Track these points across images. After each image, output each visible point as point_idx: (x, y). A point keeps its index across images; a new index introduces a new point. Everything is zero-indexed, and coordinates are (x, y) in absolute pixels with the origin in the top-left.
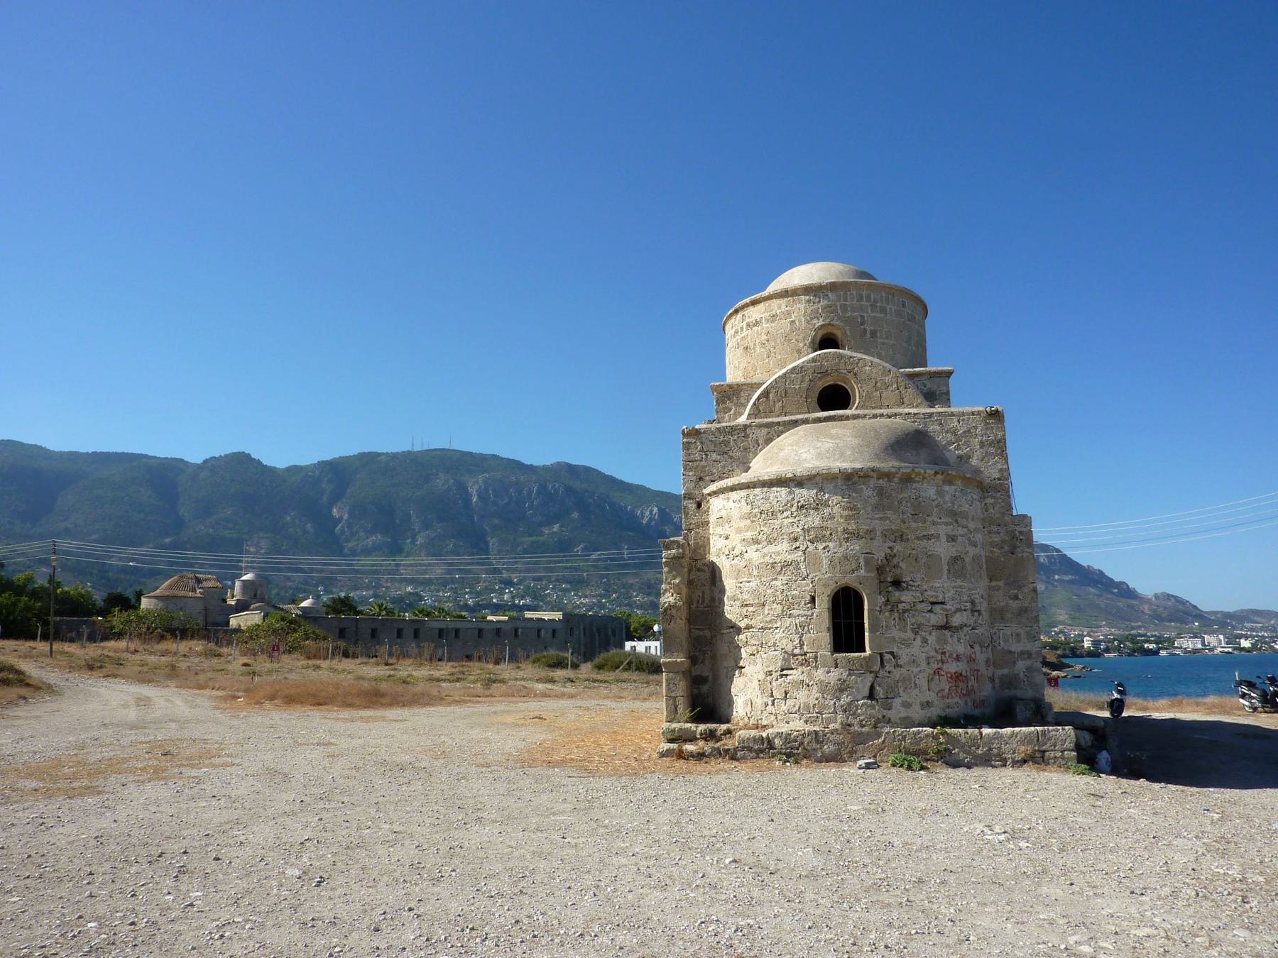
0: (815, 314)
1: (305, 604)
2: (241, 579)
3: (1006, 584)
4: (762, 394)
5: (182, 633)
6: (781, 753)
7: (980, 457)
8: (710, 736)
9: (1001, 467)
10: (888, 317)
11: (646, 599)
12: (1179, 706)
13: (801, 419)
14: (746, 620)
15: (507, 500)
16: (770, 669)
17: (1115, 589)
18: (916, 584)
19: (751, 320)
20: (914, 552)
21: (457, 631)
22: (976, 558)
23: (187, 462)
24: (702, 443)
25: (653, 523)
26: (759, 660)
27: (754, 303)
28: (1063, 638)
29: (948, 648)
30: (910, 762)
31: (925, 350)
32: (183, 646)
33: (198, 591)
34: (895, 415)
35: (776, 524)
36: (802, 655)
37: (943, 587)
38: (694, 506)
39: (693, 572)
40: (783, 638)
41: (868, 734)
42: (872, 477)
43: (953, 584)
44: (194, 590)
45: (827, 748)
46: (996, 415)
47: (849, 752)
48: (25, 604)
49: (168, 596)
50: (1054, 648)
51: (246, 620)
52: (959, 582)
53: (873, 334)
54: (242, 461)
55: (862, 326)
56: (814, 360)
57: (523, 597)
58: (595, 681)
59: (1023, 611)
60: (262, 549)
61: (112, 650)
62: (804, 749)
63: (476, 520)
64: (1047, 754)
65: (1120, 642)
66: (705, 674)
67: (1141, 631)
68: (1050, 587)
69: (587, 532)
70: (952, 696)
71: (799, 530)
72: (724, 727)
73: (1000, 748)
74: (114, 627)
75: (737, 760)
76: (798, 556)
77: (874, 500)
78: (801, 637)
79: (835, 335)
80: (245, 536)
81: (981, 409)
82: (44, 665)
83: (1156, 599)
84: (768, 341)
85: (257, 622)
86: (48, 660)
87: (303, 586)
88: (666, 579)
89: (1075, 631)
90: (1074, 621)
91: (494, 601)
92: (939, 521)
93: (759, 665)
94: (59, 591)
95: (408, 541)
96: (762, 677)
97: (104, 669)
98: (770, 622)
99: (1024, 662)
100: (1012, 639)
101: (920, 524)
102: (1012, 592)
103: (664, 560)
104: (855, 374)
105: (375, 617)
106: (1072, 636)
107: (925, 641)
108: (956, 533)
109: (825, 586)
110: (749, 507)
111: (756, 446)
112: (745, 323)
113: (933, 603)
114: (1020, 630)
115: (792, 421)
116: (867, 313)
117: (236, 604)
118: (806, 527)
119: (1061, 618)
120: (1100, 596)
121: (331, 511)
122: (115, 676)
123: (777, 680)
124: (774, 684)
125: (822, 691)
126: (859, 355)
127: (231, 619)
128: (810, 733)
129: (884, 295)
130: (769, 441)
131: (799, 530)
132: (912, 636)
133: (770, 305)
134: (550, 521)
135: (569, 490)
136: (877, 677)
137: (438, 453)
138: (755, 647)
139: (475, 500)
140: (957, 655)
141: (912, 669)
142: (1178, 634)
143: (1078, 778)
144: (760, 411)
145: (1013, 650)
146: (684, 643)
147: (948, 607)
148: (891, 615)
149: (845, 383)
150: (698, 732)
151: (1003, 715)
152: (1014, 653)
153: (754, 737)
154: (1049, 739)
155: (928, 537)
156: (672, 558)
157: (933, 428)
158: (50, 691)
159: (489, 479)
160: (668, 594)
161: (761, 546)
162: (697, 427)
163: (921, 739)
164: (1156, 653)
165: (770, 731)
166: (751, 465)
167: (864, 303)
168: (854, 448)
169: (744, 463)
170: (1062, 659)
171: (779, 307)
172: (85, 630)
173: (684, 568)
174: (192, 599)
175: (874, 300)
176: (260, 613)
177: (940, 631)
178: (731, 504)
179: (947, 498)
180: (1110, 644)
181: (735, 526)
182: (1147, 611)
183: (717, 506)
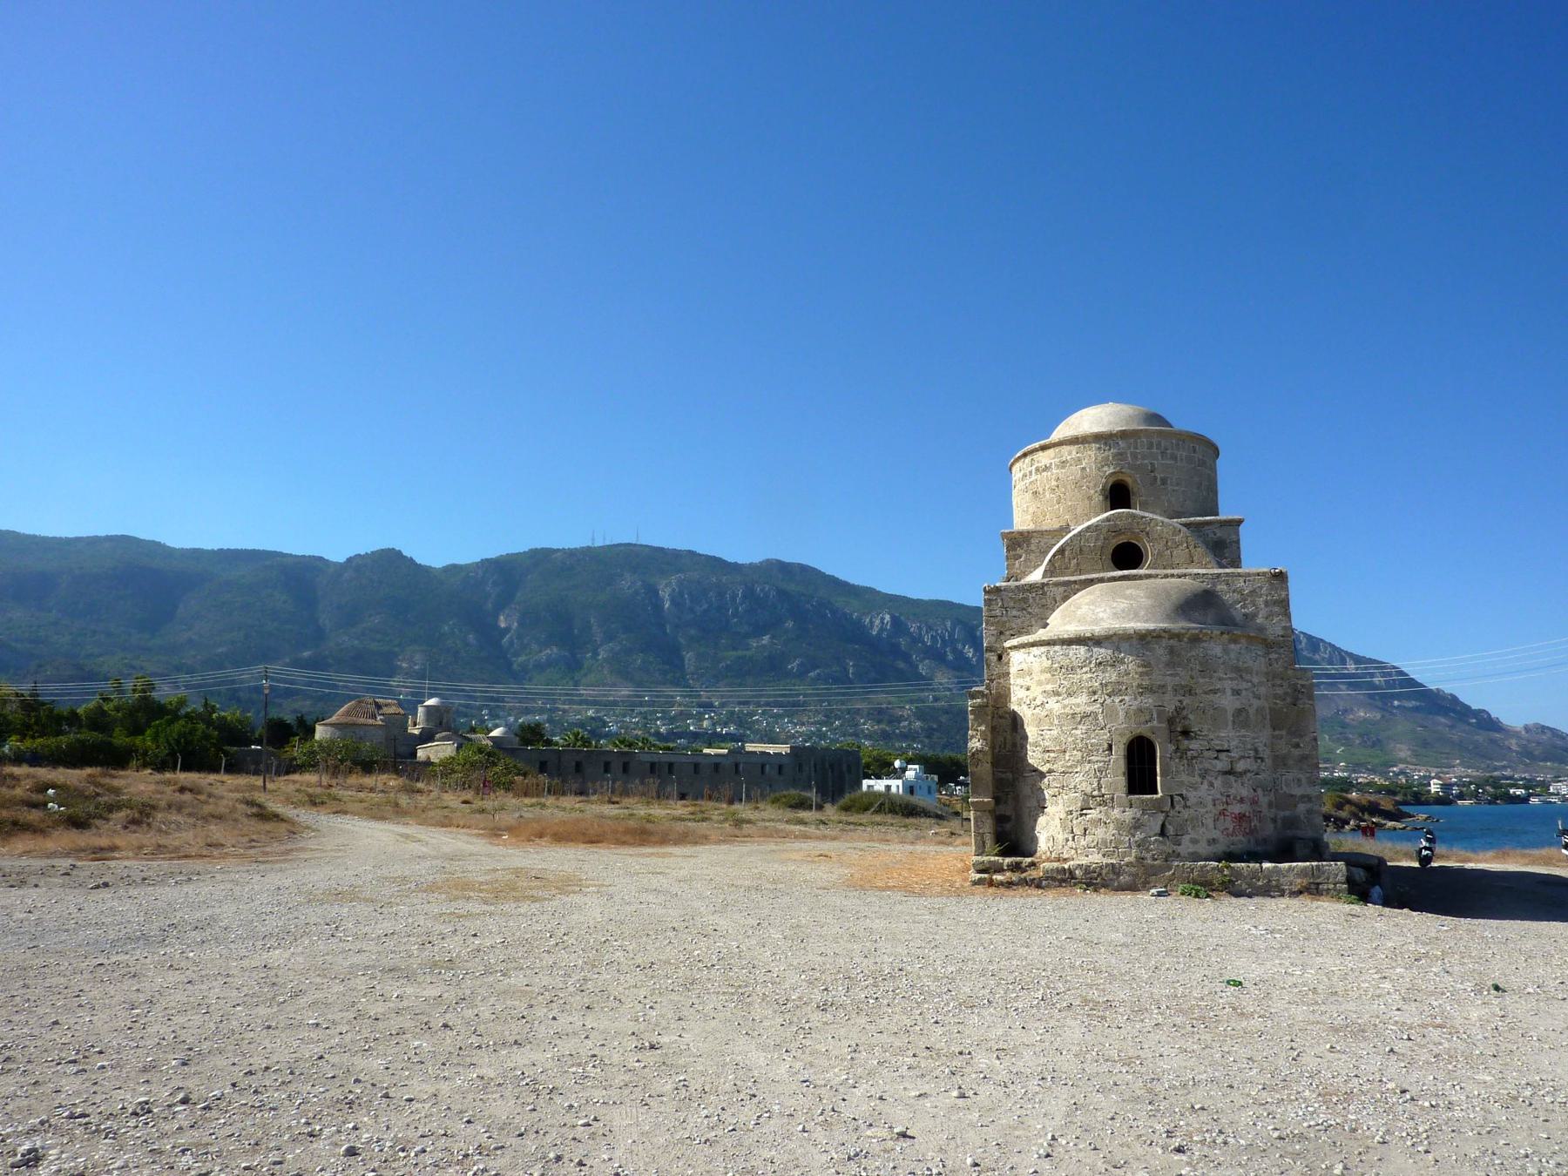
0: (1105, 462)
1: (496, 733)
2: (425, 704)
4: (1057, 551)
5: (367, 767)
6: (1081, 883)
8: (1016, 868)
9: (1284, 625)
10: (1179, 464)
11: (876, 727)
12: (1503, 857)
14: (1048, 765)
15: (705, 606)
16: (1071, 809)
17: (1472, 718)
19: (1040, 465)
20: (1201, 705)
21: (671, 765)
22: (1259, 710)
25: (884, 635)
26: (1060, 801)
27: (1043, 448)
28: (1404, 781)
29: (1232, 791)
30: (1197, 891)
31: (1216, 493)
33: (379, 718)
34: (1185, 575)
35: (1076, 678)
36: (1100, 797)
37: (1227, 735)
38: (996, 658)
39: (995, 719)
40: (1082, 781)
42: (1165, 637)
43: (1238, 734)
44: (374, 717)
46: (1280, 577)
48: (203, 732)
49: (346, 724)
50: (1391, 791)
51: (437, 752)
52: (1243, 732)
53: (1164, 482)
54: (390, 562)
56: (1108, 519)
57: (725, 725)
58: (850, 823)
59: (1304, 758)
60: (415, 665)
61: (305, 784)
62: (1102, 879)
63: (668, 631)
64: (1321, 887)
65: (1478, 787)
66: (1008, 813)
67: (1507, 773)
68: (1387, 715)
71: (1097, 684)
72: (1029, 860)
74: (295, 759)
75: (1043, 888)
76: (1096, 707)
79: (1126, 482)
80: (396, 649)
81: (1265, 570)
83: (1527, 732)
84: (1058, 487)
87: (464, 709)
88: (972, 726)
89: (1419, 771)
90: (1419, 759)
91: (691, 728)
93: (1061, 806)
95: (589, 655)
96: (1063, 816)
98: (1071, 766)
99: (1304, 805)
100: (1293, 784)
102: (1294, 740)
103: (970, 708)
104: (1148, 534)
105: (571, 748)
106: (1416, 777)
107: (1211, 785)
108: (1240, 687)
110: (1050, 662)
111: (1053, 602)
112: (1034, 467)
113: (1218, 751)
114: (1301, 776)
116: (1157, 460)
117: (421, 733)
119: (1402, 755)
120: (1452, 727)
123: (1077, 818)
124: (1074, 822)
125: (1119, 829)
126: (1151, 515)
128: (1107, 865)
129: (1174, 441)
130: (1065, 598)
132: (1199, 780)
134: (759, 631)
135: (783, 594)
137: (622, 548)
138: (1056, 790)
139: (667, 606)
141: (1200, 810)
142: (1555, 777)
143: (1346, 906)
145: (1294, 793)
146: (990, 784)
147: (1232, 754)
148: (1180, 761)
150: (1005, 864)
151: (1284, 852)
152: (1295, 796)
153: (1057, 869)
154: (1323, 873)
155: (1215, 692)
157: (1221, 587)
159: (684, 580)
160: (974, 740)
161: (1061, 698)
162: (997, 585)
163: (1208, 872)
164: (1524, 800)
165: (1072, 863)
166: (1048, 621)
169: (1042, 619)
170: (1401, 807)
171: (1070, 454)
173: (987, 715)
174: (372, 728)
176: (453, 744)
177: (1225, 776)
178: (1031, 658)
179: (1233, 655)
180: (1465, 789)
181: (1036, 678)
182: (1514, 747)
183: (1017, 660)
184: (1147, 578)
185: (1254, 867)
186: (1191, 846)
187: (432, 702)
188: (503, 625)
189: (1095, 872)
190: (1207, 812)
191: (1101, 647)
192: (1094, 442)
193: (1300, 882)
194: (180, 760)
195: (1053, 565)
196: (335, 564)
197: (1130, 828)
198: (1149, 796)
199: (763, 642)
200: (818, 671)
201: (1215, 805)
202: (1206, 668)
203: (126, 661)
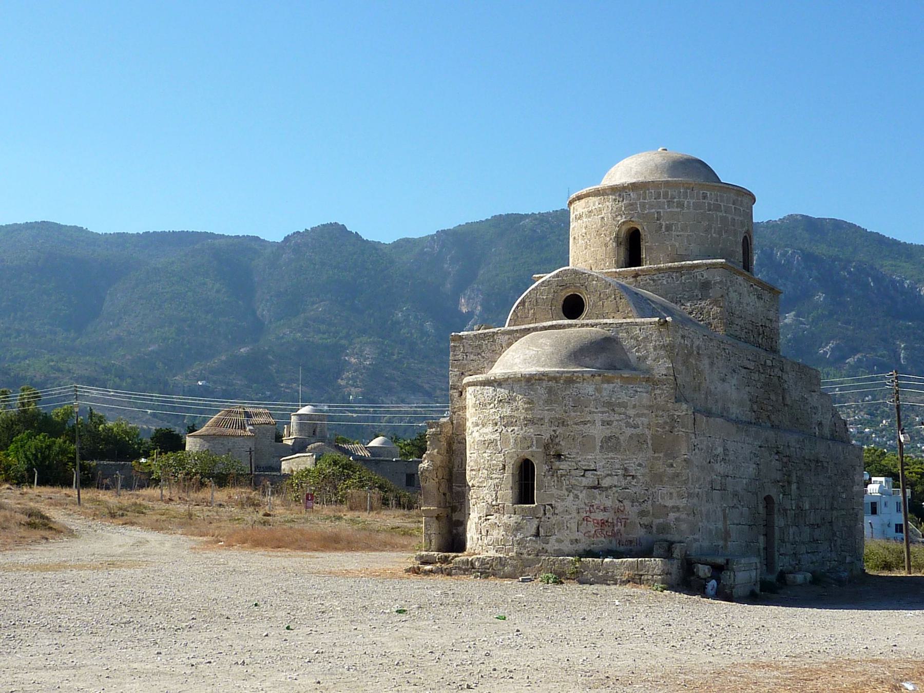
0: (618, 213)
1: (376, 443)
2: (299, 412)
3: (666, 455)
5: (222, 481)
7: (654, 358)
9: (667, 366)
10: (686, 210)
13: (532, 328)
18: (572, 456)
20: (572, 434)
23: (264, 241)
24: (464, 346)
29: (596, 502)
32: (221, 495)
34: (596, 325)
37: (595, 458)
41: (532, 560)
43: (605, 457)
44: (243, 427)
45: (507, 569)
47: (520, 572)
51: (298, 464)
52: (611, 455)
53: (668, 228)
55: (658, 222)
61: (146, 499)
62: (493, 569)
64: (642, 577)
69: (840, 324)
70: (597, 536)
73: (613, 572)
76: (496, 436)
77: (545, 396)
78: (496, 493)
80: (343, 342)
82: (71, 513)
84: (586, 234)
85: (308, 467)
86: (77, 508)
92: (595, 410)
94: (101, 427)
97: (125, 517)
99: (674, 514)
101: (579, 413)
104: (586, 287)
109: (511, 458)
111: (501, 348)
113: (586, 470)
114: (672, 491)
115: (526, 329)
116: (664, 208)
118: (502, 416)
121: (457, 302)
122: (132, 524)
125: (505, 531)
127: (283, 463)
131: (497, 417)
132: (566, 493)
133: (588, 202)
135: (809, 258)
136: (541, 521)
140: (604, 508)
144: (518, 317)
145: (667, 505)
148: (551, 479)
149: (580, 293)
154: (645, 567)
155: (585, 423)
156: (432, 435)
157: (622, 335)
158: (70, 534)
163: (565, 564)
167: (662, 200)
168: (547, 355)
172: (119, 476)
175: (671, 196)
176: (312, 455)
184: (569, 327)
185: (597, 561)
186: (556, 544)
187: (305, 410)
188: (464, 310)
189: (488, 564)
190: (571, 518)
191: (501, 388)
192: (611, 194)
193: (627, 573)
194: (36, 474)
195: (517, 314)
196: (274, 244)
197: (514, 531)
198: (527, 506)
199: (786, 321)
200: (858, 356)
201: (578, 513)
202: (578, 403)
203: (52, 364)
